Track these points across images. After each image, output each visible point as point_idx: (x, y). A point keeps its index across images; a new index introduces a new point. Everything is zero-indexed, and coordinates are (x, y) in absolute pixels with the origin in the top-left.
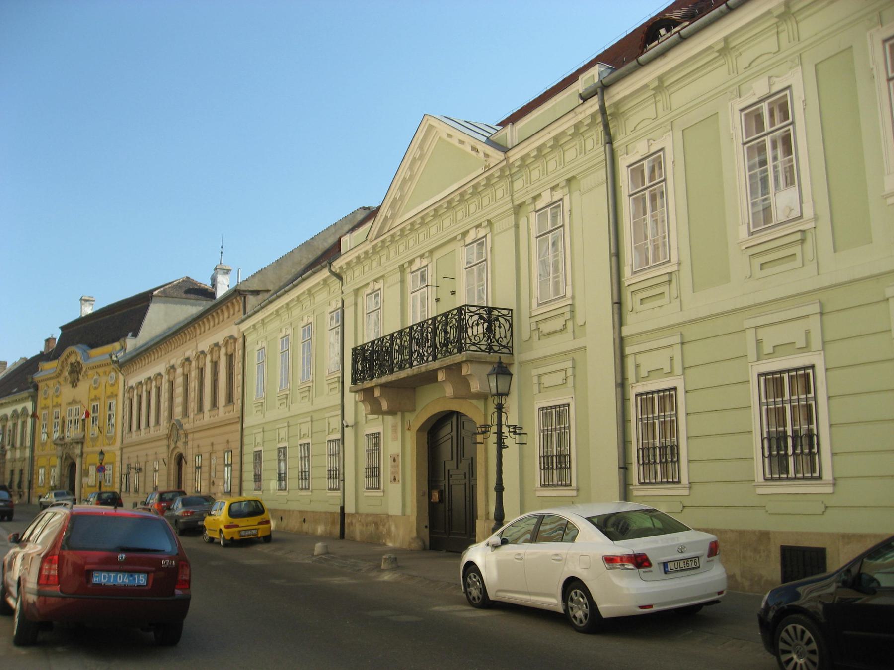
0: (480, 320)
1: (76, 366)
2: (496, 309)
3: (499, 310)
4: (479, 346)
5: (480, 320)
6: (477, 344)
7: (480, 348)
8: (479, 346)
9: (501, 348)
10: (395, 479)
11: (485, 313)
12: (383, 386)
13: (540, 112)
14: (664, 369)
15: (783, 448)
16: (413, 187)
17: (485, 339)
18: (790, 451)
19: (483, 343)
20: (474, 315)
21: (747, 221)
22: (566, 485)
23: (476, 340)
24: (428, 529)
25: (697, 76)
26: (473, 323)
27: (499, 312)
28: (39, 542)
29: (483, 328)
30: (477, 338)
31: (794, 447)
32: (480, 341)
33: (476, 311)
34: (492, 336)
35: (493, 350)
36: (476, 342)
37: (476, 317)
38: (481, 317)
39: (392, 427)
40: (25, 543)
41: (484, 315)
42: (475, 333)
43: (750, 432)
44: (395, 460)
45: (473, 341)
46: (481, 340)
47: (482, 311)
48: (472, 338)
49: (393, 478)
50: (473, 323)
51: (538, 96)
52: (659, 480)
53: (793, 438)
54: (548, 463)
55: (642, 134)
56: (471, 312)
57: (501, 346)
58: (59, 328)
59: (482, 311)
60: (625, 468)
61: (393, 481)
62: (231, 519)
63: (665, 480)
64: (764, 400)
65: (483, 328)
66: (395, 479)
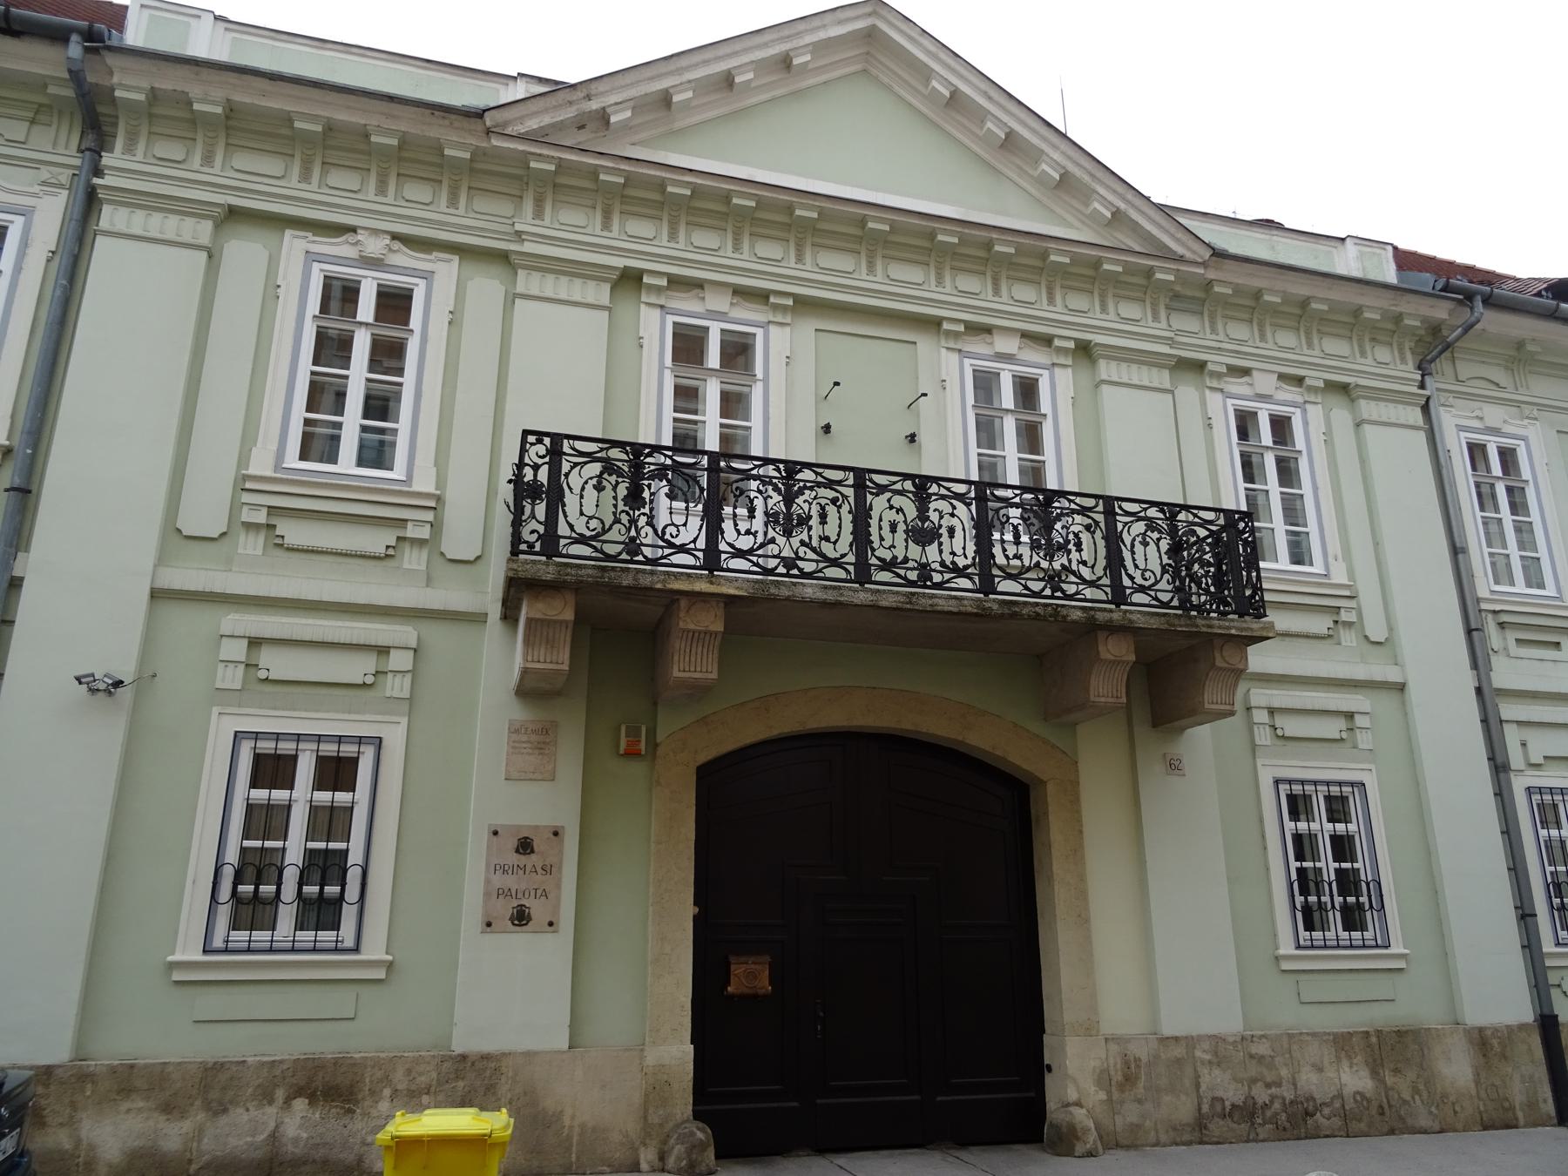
0: (605, 476)
1: (77, 1165)
2: (1187, 508)
3: (1195, 511)
4: (1152, 593)
5: (605, 476)
6: (1149, 588)
7: (1156, 599)
8: (1152, 593)
9: (822, 565)
11: (1161, 516)
14: (277, 529)
17: (1167, 576)
19: (1163, 585)
20: (586, 463)
21: (1507, 429)
23: (1146, 579)
26: (1134, 540)
27: (817, 474)
29: (1159, 550)
30: (1147, 574)
32: (1157, 582)
33: (1013, 498)
34: (643, 520)
35: (1063, 591)
36: (1147, 584)
37: (596, 468)
38: (1151, 525)
41: (1160, 522)
42: (589, 509)
43: (239, 707)
45: (1139, 580)
46: (1158, 579)
47: (615, 453)
48: (1137, 575)
50: (1134, 540)
56: (1127, 514)
57: (671, 545)
58: (1274, 778)
60: (1525, 916)
65: (1159, 550)
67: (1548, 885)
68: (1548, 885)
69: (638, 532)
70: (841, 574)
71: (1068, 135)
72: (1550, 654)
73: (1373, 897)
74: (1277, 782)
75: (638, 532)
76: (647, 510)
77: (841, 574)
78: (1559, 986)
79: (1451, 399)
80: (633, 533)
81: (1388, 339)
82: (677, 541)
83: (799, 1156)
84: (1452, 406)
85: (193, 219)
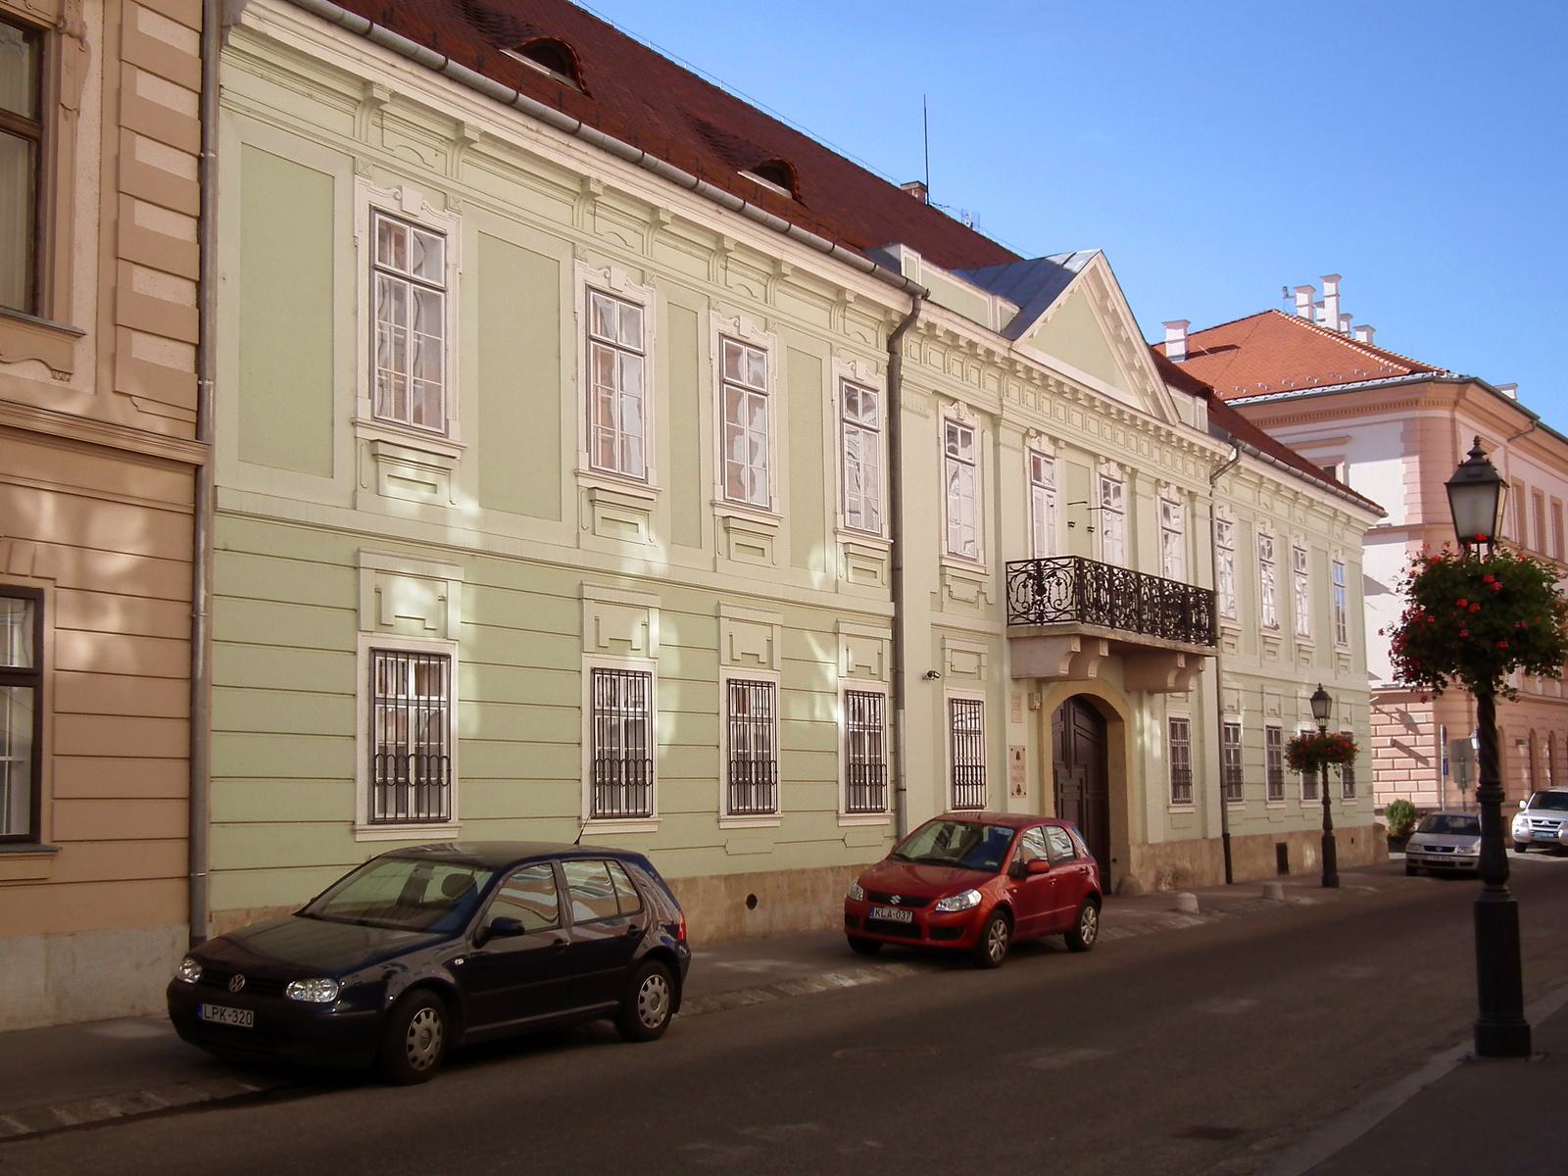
10: (1019, 791)
12: (1112, 643)
13: (969, 290)
15: (426, 773)
16: (1089, 299)
18: (412, 779)
22: (439, 820)
24: (1111, 858)
25: (522, 180)
28: (1012, 353)
31: (418, 774)
34: (1046, 600)
39: (1013, 698)
40: (375, 110)
44: (1018, 757)
49: (1016, 788)
51: (635, 38)
52: (754, 807)
53: (396, 759)
54: (604, 772)
55: (511, 213)
57: (1059, 610)
59: (1030, 567)
61: (1015, 793)
62: (181, 1040)
63: (400, 815)
64: (444, 710)
66: (1019, 791)
67: (731, 762)
68: (731, 762)
69: (1044, 606)
70: (1068, 617)
71: (1351, 487)
72: (757, 559)
73: (426, 768)
74: (729, 681)
75: (1044, 606)
76: (1047, 594)
77: (1068, 617)
78: (843, 840)
79: (370, 168)
80: (1042, 608)
81: (707, 257)
82: (1061, 608)
83: (386, 902)
84: (369, 177)
85: (76, 255)
